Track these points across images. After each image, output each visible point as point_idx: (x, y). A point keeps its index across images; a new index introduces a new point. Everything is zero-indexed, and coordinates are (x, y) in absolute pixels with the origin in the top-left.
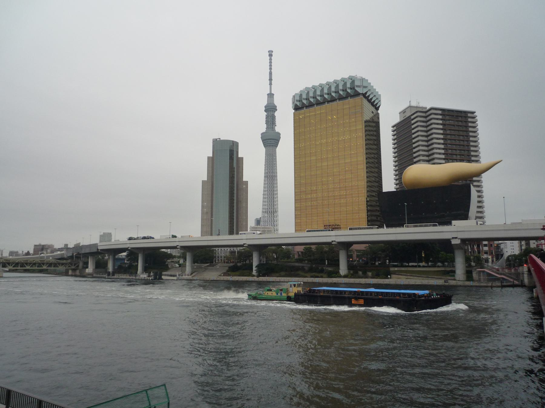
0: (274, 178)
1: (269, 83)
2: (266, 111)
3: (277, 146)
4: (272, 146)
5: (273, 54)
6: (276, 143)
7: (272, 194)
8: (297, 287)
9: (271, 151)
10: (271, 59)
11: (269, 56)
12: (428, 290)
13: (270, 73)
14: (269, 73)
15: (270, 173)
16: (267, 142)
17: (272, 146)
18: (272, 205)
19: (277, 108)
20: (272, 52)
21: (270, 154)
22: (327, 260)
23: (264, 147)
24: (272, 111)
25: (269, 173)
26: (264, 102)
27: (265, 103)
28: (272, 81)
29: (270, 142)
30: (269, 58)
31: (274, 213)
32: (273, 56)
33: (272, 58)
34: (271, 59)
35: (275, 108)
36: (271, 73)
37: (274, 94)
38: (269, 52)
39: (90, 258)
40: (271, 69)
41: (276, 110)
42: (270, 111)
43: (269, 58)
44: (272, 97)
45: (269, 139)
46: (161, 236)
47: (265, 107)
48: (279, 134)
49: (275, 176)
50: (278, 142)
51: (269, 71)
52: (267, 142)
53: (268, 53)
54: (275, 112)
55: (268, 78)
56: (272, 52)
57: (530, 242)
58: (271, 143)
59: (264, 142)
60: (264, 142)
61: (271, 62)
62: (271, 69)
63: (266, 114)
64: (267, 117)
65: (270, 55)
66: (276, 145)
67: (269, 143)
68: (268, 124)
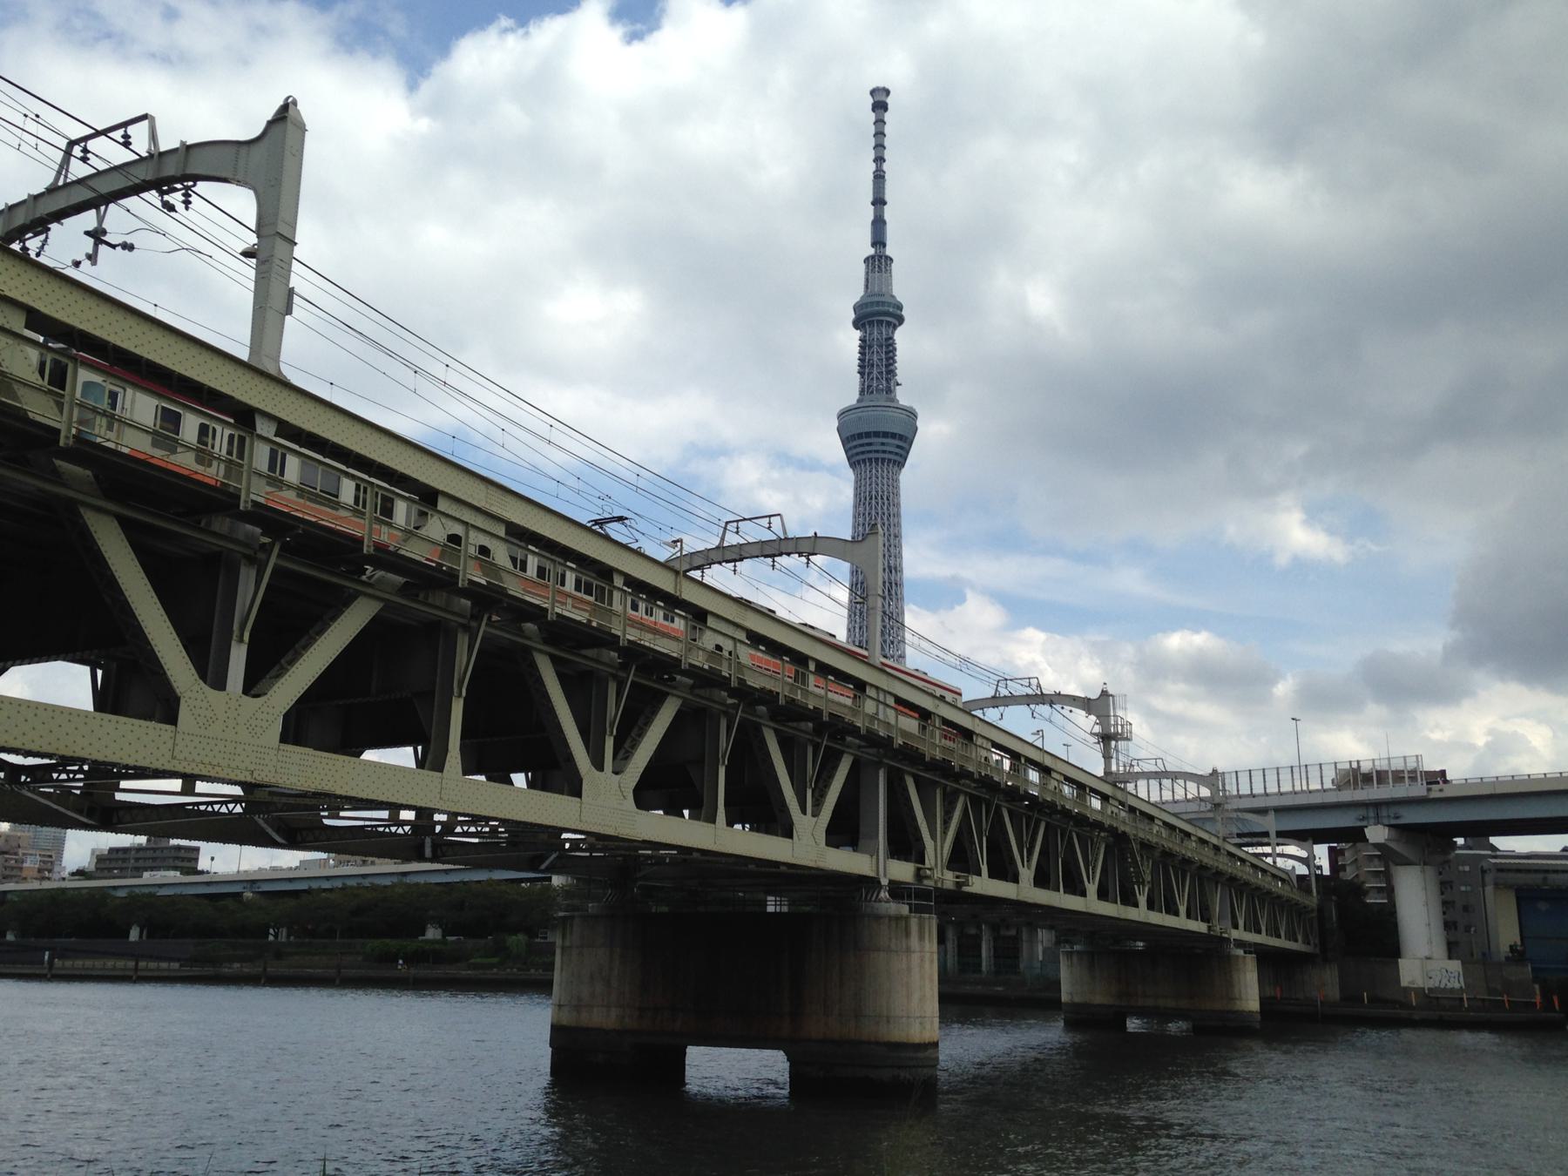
0: (893, 592)
1: (871, 199)
2: (857, 324)
4: (883, 464)
5: (889, 100)
6: (897, 450)
7: (884, 504)
9: (885, 481)
11: (873, 110)
16: (870, 444)
17: (883, 464)
18: (884, 514)
19: (127, 251)
20: (887, 92)
21: (877, 492)
23: (851, 465)
24: (889, 323)
27: (857, 292)
29: (883, 444)
30: (872, 117)
31: (891, 572)
33: (887, 117)
35: (899, 312)
37: (891, 260)
40: (879, 160)
42: (880, 322)
43: (874, 120)
44: (880, 270)
45: (877, 434)
47: (857, 308)
49: (896, 584)
50: (907, 447)
51: (873, 167)
52: (870, 444)
53: (871, 101)
54: (895, 327)
58: (884, 452)
59: (849, 446)
60: (850, 453)
63: (858, 334)
65: (880, 106)
66: (900, 460)
67: (877, 451)
68: (869, 374)
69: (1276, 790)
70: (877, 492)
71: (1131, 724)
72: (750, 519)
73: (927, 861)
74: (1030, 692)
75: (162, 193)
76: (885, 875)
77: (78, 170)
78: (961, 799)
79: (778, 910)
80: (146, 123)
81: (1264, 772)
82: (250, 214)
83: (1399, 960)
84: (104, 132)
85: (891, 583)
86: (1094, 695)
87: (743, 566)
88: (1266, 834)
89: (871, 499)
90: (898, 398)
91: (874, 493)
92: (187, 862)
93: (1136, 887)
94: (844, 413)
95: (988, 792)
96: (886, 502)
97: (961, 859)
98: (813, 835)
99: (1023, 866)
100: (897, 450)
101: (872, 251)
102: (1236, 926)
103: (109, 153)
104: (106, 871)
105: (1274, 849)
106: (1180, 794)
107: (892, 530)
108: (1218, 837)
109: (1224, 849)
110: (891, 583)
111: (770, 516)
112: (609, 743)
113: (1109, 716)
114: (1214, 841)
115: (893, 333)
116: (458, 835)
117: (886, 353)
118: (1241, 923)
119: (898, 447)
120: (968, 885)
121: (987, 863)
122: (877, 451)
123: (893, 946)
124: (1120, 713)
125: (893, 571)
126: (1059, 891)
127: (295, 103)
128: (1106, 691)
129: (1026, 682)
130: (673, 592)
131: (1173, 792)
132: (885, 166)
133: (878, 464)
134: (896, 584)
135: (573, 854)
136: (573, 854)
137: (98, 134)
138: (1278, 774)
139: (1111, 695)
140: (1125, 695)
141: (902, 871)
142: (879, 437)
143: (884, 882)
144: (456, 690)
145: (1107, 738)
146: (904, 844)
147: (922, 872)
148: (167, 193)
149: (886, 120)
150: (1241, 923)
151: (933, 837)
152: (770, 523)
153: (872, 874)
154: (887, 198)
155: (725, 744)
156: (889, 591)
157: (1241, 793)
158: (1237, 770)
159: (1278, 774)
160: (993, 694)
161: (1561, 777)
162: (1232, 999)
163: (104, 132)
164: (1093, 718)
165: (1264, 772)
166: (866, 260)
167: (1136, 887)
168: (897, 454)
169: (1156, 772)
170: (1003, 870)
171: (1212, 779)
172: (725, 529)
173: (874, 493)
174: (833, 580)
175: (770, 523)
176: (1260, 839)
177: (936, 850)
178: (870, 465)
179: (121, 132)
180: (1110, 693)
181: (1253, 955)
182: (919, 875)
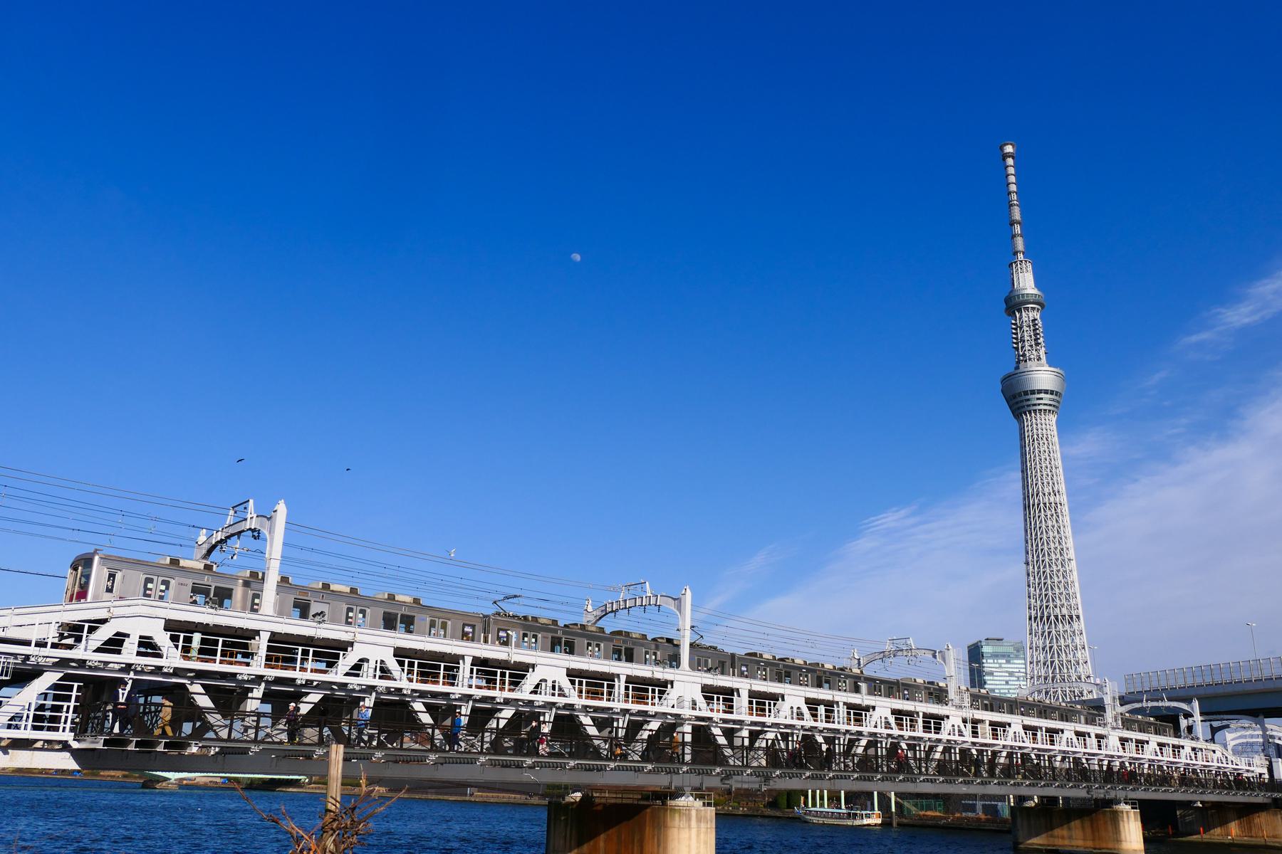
0: (1059, 511)
31: (1055, 495)
70: (1038, 435)
91: (1035, 436)
94: (1005, 379)
104: (237, 752)
107: (1052, 463)
116: (631, 761)
117: (1035, 340)
123: (682, 826)
125: (1057, 494)
133: (1036, 415)
134: (1061, 504)
135: (154, 773)
136: (154, 773)
142: (1047, 393)
156: (1055, 510)
161: (1277, 671)
162: (1119, 841)
168: (1050, 405)
173: (1035, 436)
174: (669, 615)
176: (1222, 716)
178: (1030, 416)
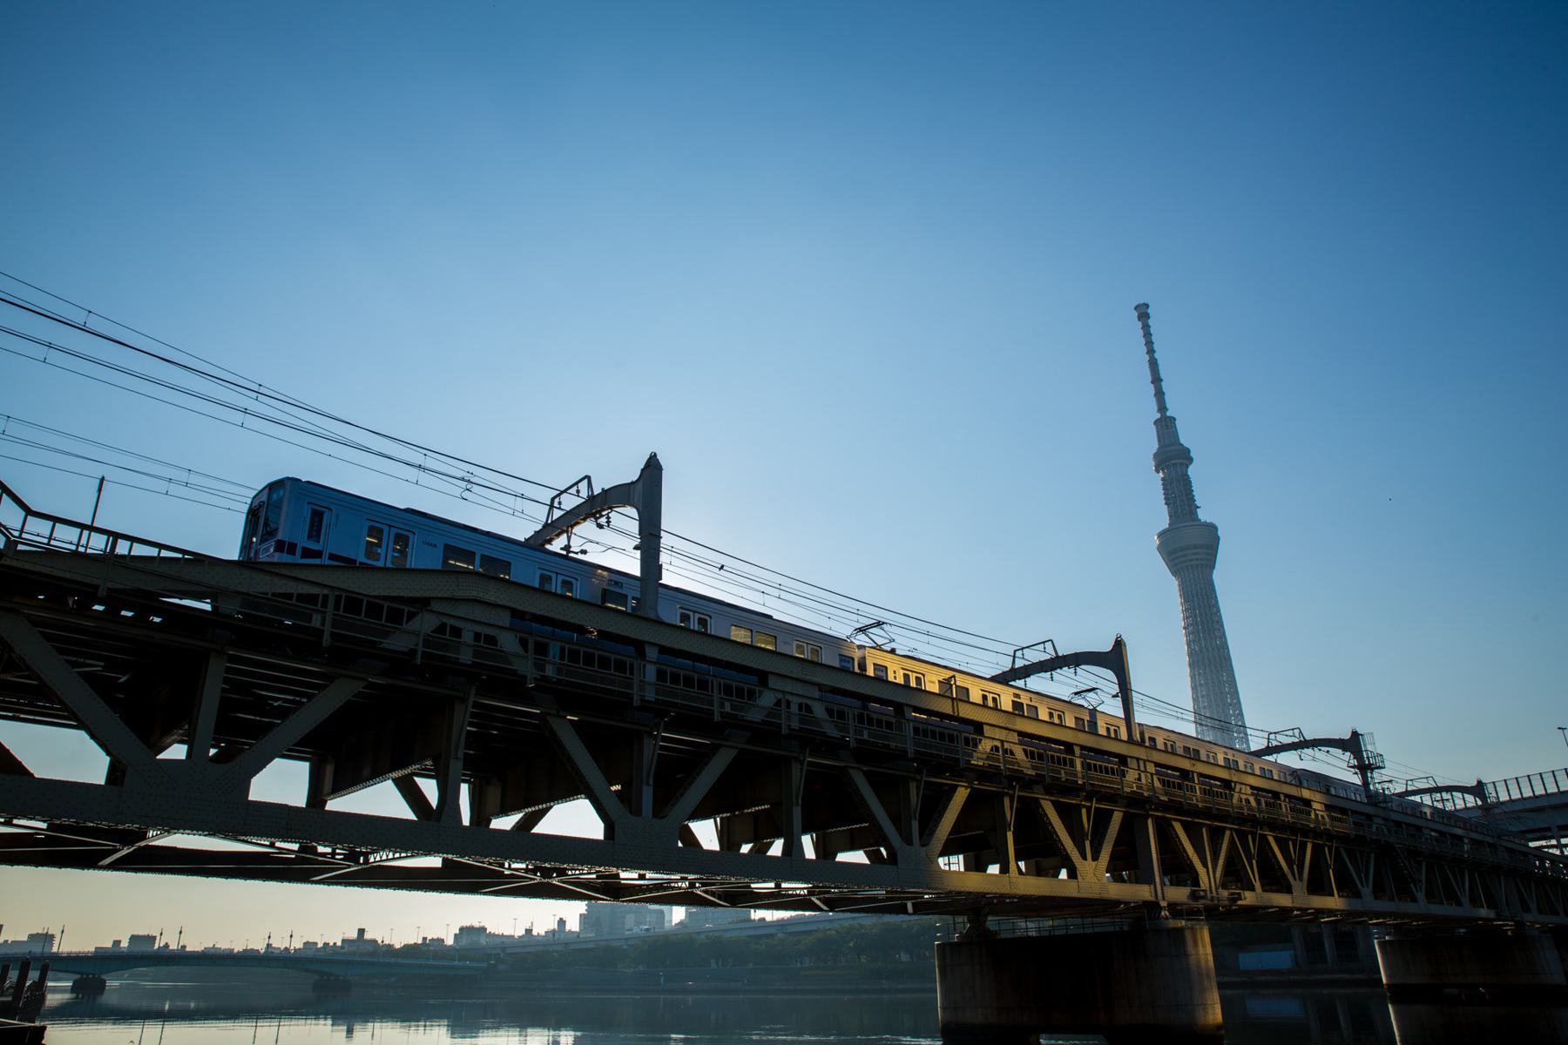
1: (1150, 379)
3: (1213, 567)
5: (1149, 311)
6: (1195, 557)
8: (1013, 701)
10: (1162, 407)
12: (644, 649)
13: (1150, 364)
14: (1147, 364)
15: (1208, 650)
16: (1185, 555)
20: (1147, 306)
22: (293, 623)
23: (1173, 575)
25: (1204, 650)
26: (1150, 443)
28: (1163, 383)
32: (1151, 315)
33: (1150, 322)
34: (1162, 407)
36: (1153, 364)
38: (1136, 308)
39: (1207, 961)
40: (1151, 351)
41: (1191, 460)
46: (510, 563)
48: (1212, 529)
51: (1147, 357)
52: (1185, 555)
55: (1149, 379)
56: (1147, 306)
57: (803, 840)
61: (1160, 395)
62: (1151, 351)
64: (1166, 483)
67: (1191, 560)
69: (1463, 806)
71: (1381, 755)
72: (1028, 647)
73: (1202, 884)
74: (1296, 740)
75: (597, 519)
76: (1164, 899)
77: (557, 514)
78: (1228, 833)
79: (1118, 929)
80: (586, 480)
81: (1541, 776)
82: (634, 527)
83: (329, 1022)
84: (565, 491)
85: (1220, 659)
86: (1347, 736)
87: (1057, 674)
88: (1549, 829)
89: (1193, 597)
90: (1200, 517)
91: (1194, 592)
92: (923, 898)
93: (1412, 885)
95: (1247, 823)
96: (1205, 597)
97: (1234, 875)
98: (1094, 874)
99: (1295, 880)
100: (1195, 557)
101: (1158, 416)
102: (1528, 910)
103: (569, 502)
105: (1558, 841)
106: (1460, 805)
108: (1493, 837)
109: (1501, 845)
110: (1220, 659)
111: (1044, 642)
112: (915, 825)
113: (1362, 751)
114: (1488, 839)
115: (1186, 471)
118: (1533, 906)
119: (1194, 554)
120: (1241, 900)
121: (1260, 879)
122: (1191, 560)
124: (1369, 748)
126: (1333, 895)
127: (655, 454)
128: (1356, 732)
129: (1290, 733)
130: (952, 713)
131: (1464, 801)
132: (1156, 355)
137: (562, 492)
138: (1554, 776)
139: (1362, 735)
140: (1372, 733)
141: (1180, 894)
143: (1163, 904)
144: (795, 801)
145: (1364, 768)
146: (1179, 870)
147: (1197, 893)
148: (599, 518)
149: (1150, 324)
150: (1533, 906)
151: (1205, 865)
152: (1045, 648)
153: (1153, 899)
154: (1162, 376)
155: (1009, 815)
157: (1561, 790)
158: (1506, 778)
159: (1554, 776)
160: (1266, 745)
163: (565, 491)
164: (1348, 754)
165: (1541, 776)
166: (1156, 423)
167: (1412, 885)
169: (1429, 789)
170: (1274, 880)
171: (1479, 789)
172: (1014, 657)
175: (1045, 648)
177: (1207, 877)
179: (575, 488)
180: (1360, 732)
181: (1549, 935)
182: (1194, 896)
